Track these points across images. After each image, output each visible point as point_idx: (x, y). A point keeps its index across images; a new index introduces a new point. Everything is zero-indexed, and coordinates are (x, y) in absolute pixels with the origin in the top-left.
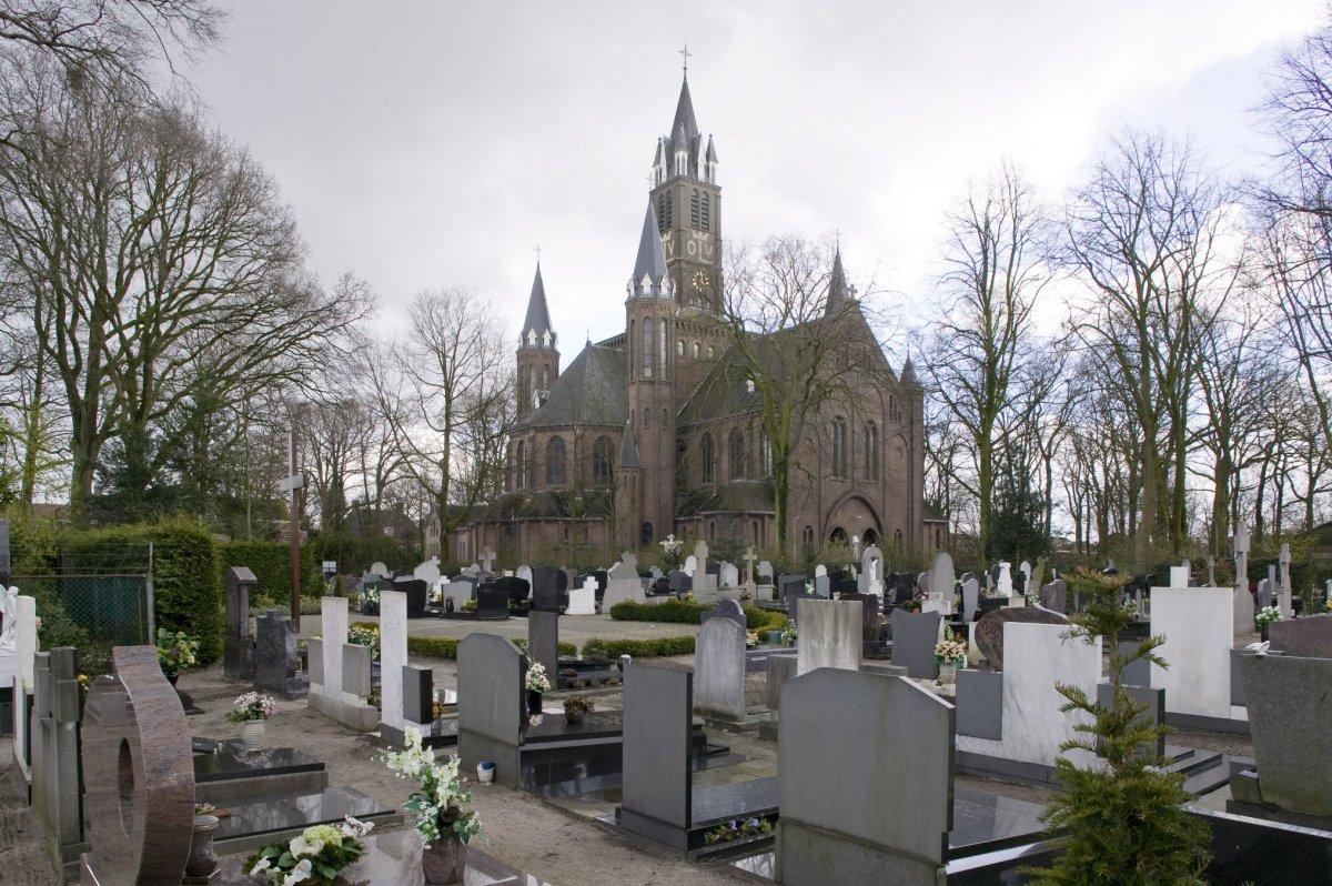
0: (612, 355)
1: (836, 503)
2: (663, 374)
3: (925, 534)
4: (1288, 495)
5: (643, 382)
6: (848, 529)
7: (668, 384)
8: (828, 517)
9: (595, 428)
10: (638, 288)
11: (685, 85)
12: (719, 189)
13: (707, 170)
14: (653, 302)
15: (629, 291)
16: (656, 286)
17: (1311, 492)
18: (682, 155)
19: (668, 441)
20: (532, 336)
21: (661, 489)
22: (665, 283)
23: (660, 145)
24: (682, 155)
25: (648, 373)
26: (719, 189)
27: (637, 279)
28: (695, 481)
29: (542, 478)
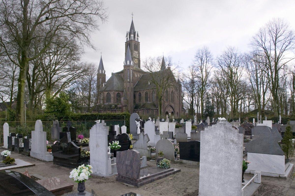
0: (119, 75)
1: (166, 107)
2: (131, 81)
3: (182, 112)
4: (245, 105)
5: (128, 82)
6: (169, 112)
7: (132, 82)
8: (165, 110)
9: (116, 91)
10: (126, 63)
11: (132, 21)
12: (139, 43)
13: (137, 38)
14: (129, 66)
15: (124, 63)
16: (130, 63)
17: (249, 105)
18: (132, 35)
19: (132, 94)
20: (100, 71)
21: (131, 105)
22: (132, 62)
23: (127, 33)
24: (132, 35)
25: (128, 80)
26: (139, 43)
27: (126, 61)
28: (137, 102)
29: (105, 101)
